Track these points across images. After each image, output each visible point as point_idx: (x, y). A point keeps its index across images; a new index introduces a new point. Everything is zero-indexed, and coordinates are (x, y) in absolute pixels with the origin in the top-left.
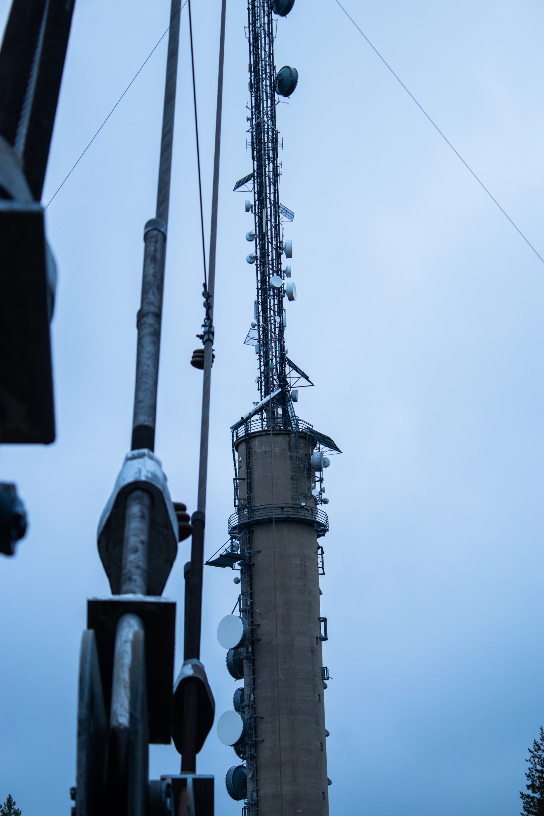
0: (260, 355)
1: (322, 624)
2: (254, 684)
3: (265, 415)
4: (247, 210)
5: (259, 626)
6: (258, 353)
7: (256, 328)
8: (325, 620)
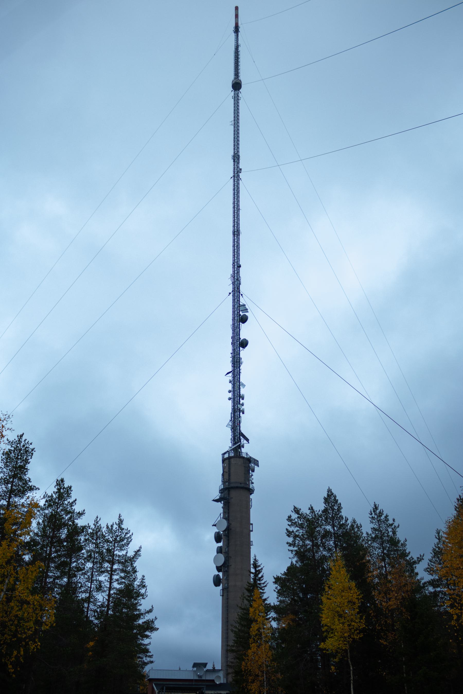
0: (232, 431)
1: (251, 526)
2: (228, 545)
3: (233, 451)
4: (230, 382)
5: (231, 524)
6: (231, 430)
7: (231, 421)
8: (252, 524)
